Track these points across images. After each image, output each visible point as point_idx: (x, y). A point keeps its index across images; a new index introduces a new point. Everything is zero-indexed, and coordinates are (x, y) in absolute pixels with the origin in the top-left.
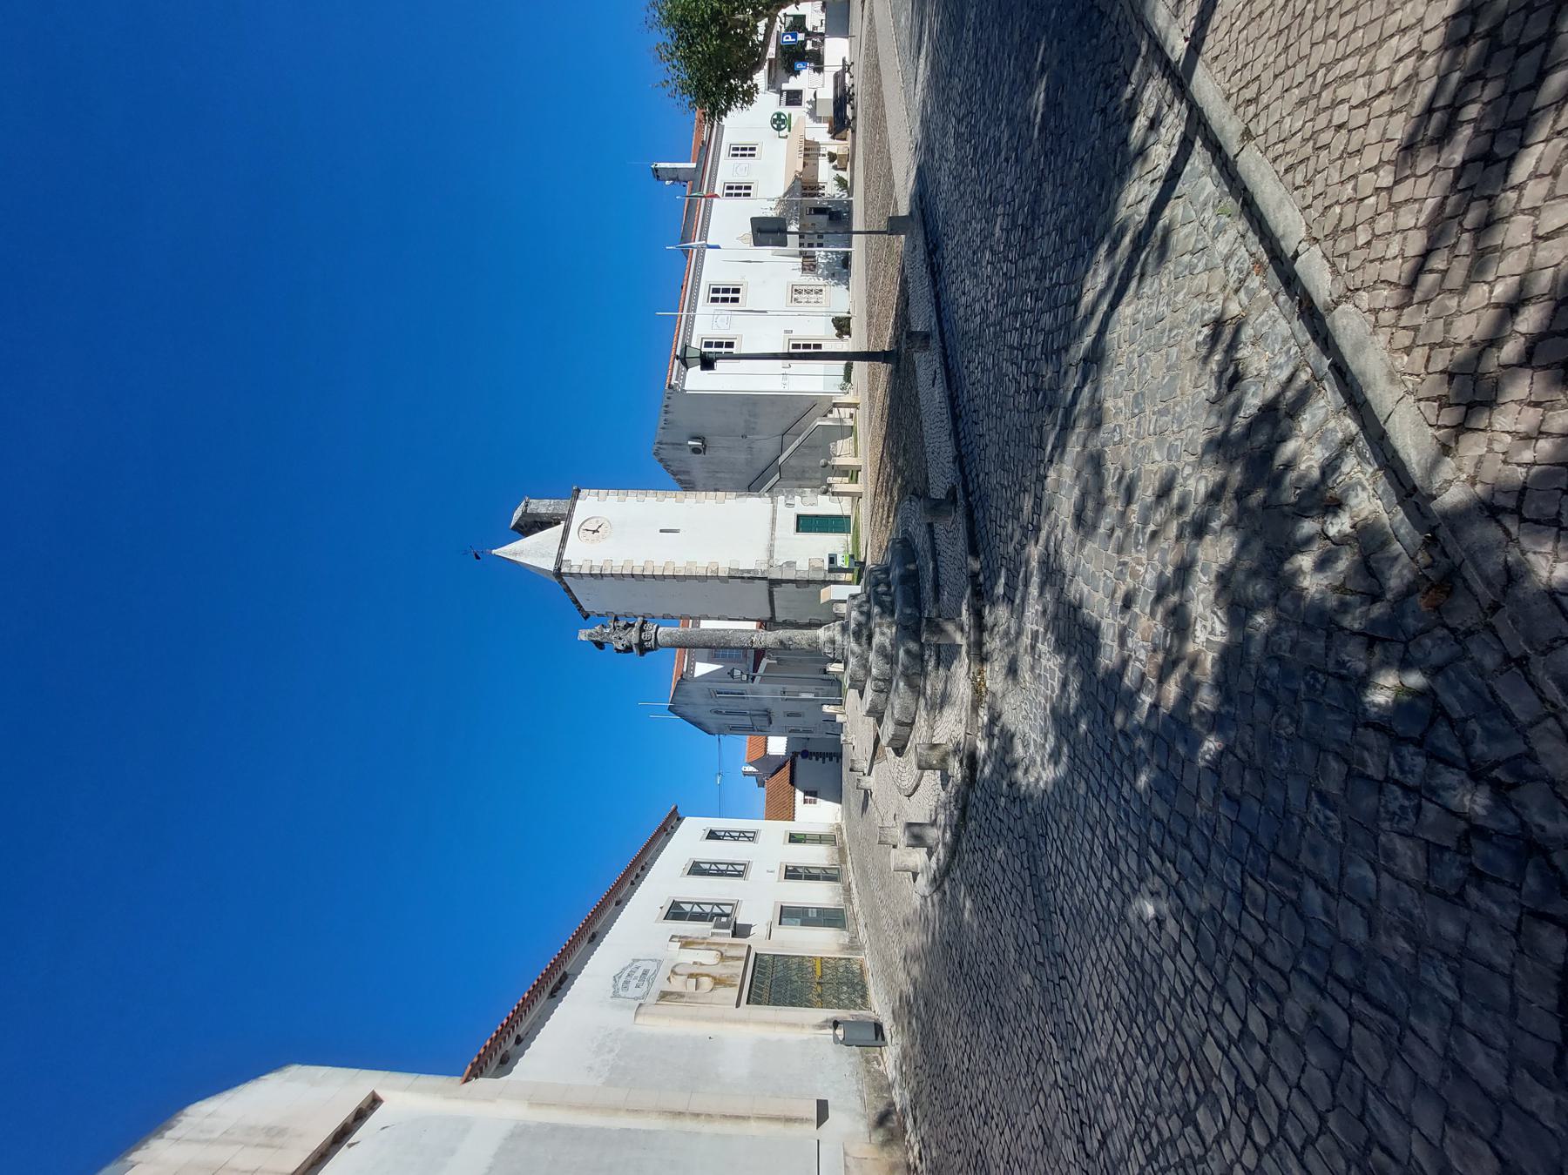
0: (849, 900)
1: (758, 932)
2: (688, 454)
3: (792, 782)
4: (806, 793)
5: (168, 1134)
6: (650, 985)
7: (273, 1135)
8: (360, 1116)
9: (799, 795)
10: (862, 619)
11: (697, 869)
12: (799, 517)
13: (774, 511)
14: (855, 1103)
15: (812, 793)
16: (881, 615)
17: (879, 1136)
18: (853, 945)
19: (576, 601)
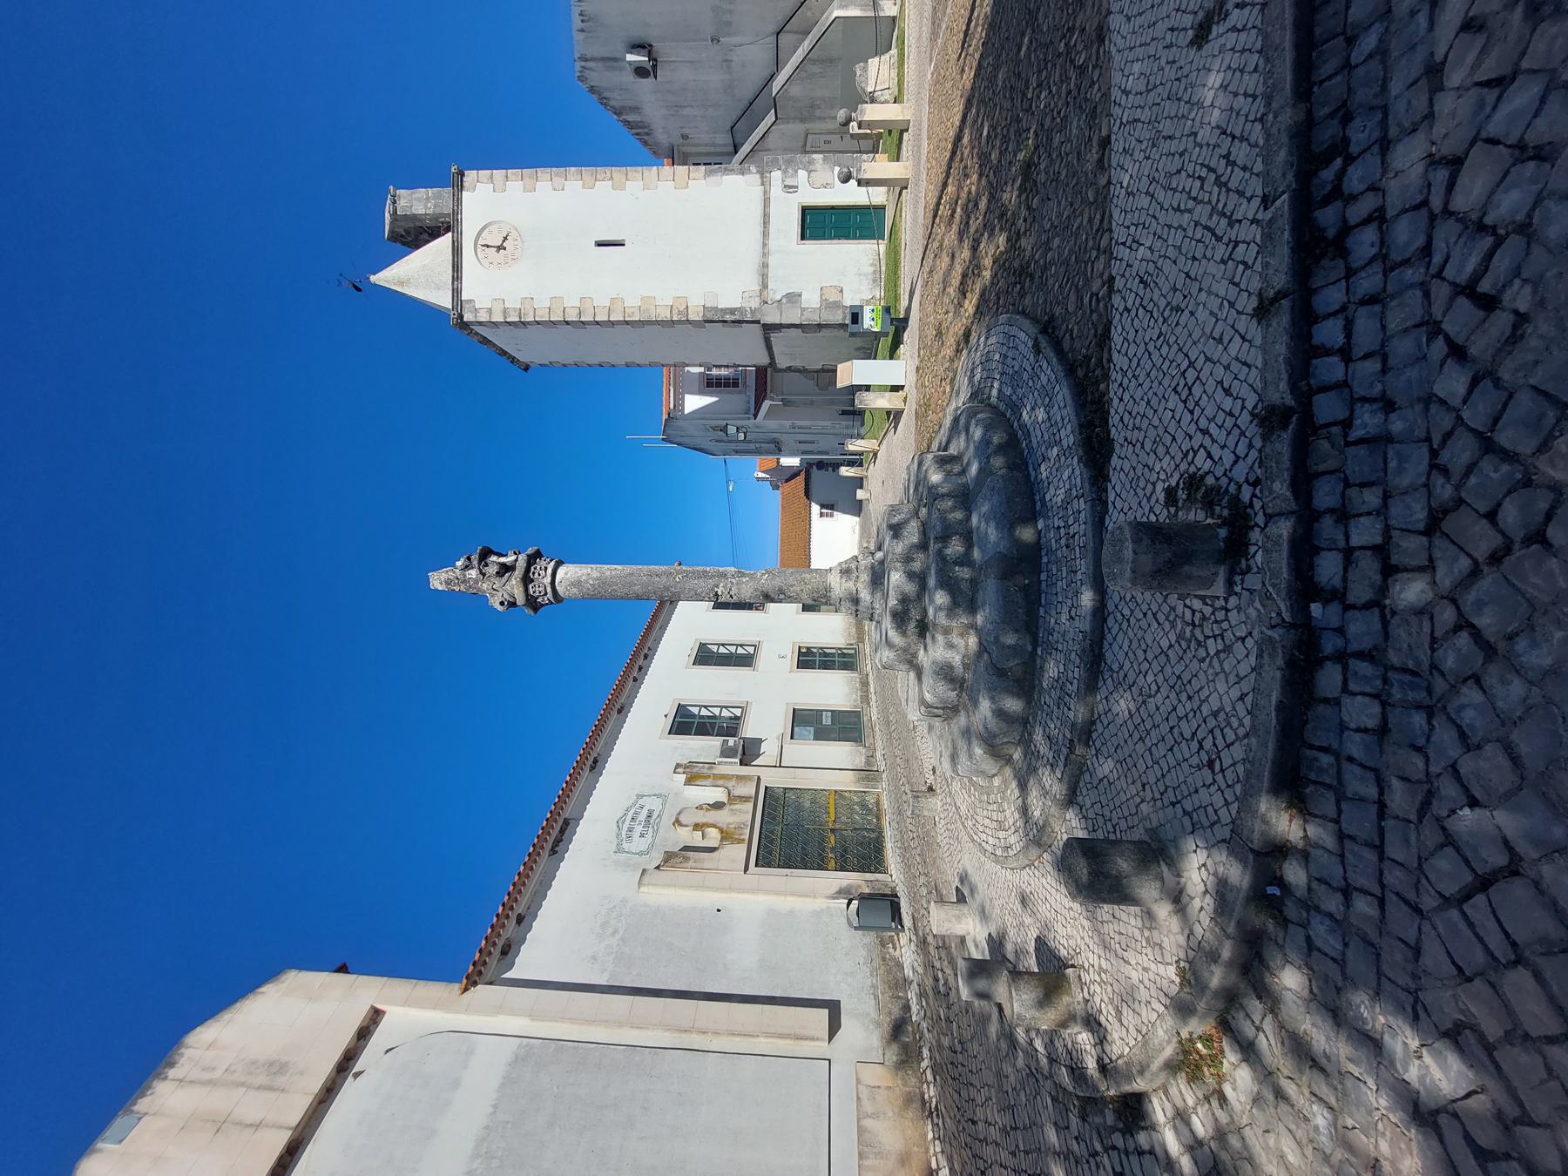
0: (866, 699)
1: (769, 751)
2: (629, 78)
3: (807, 494)
4: (822, 506)
5: (172, 1073)
6: (656, 832)
7: (277, 1070)
8: (364, 1034)
9: (815, 508)
10: (911, 588)
11: (705, 656)
12: (805, 211)
13: (766, 201)
14: (869, 1006)
15: (829, 507)
16: (951, 612)
17: (892, 1055)
18: (868, 773)
19: (503, 353)
